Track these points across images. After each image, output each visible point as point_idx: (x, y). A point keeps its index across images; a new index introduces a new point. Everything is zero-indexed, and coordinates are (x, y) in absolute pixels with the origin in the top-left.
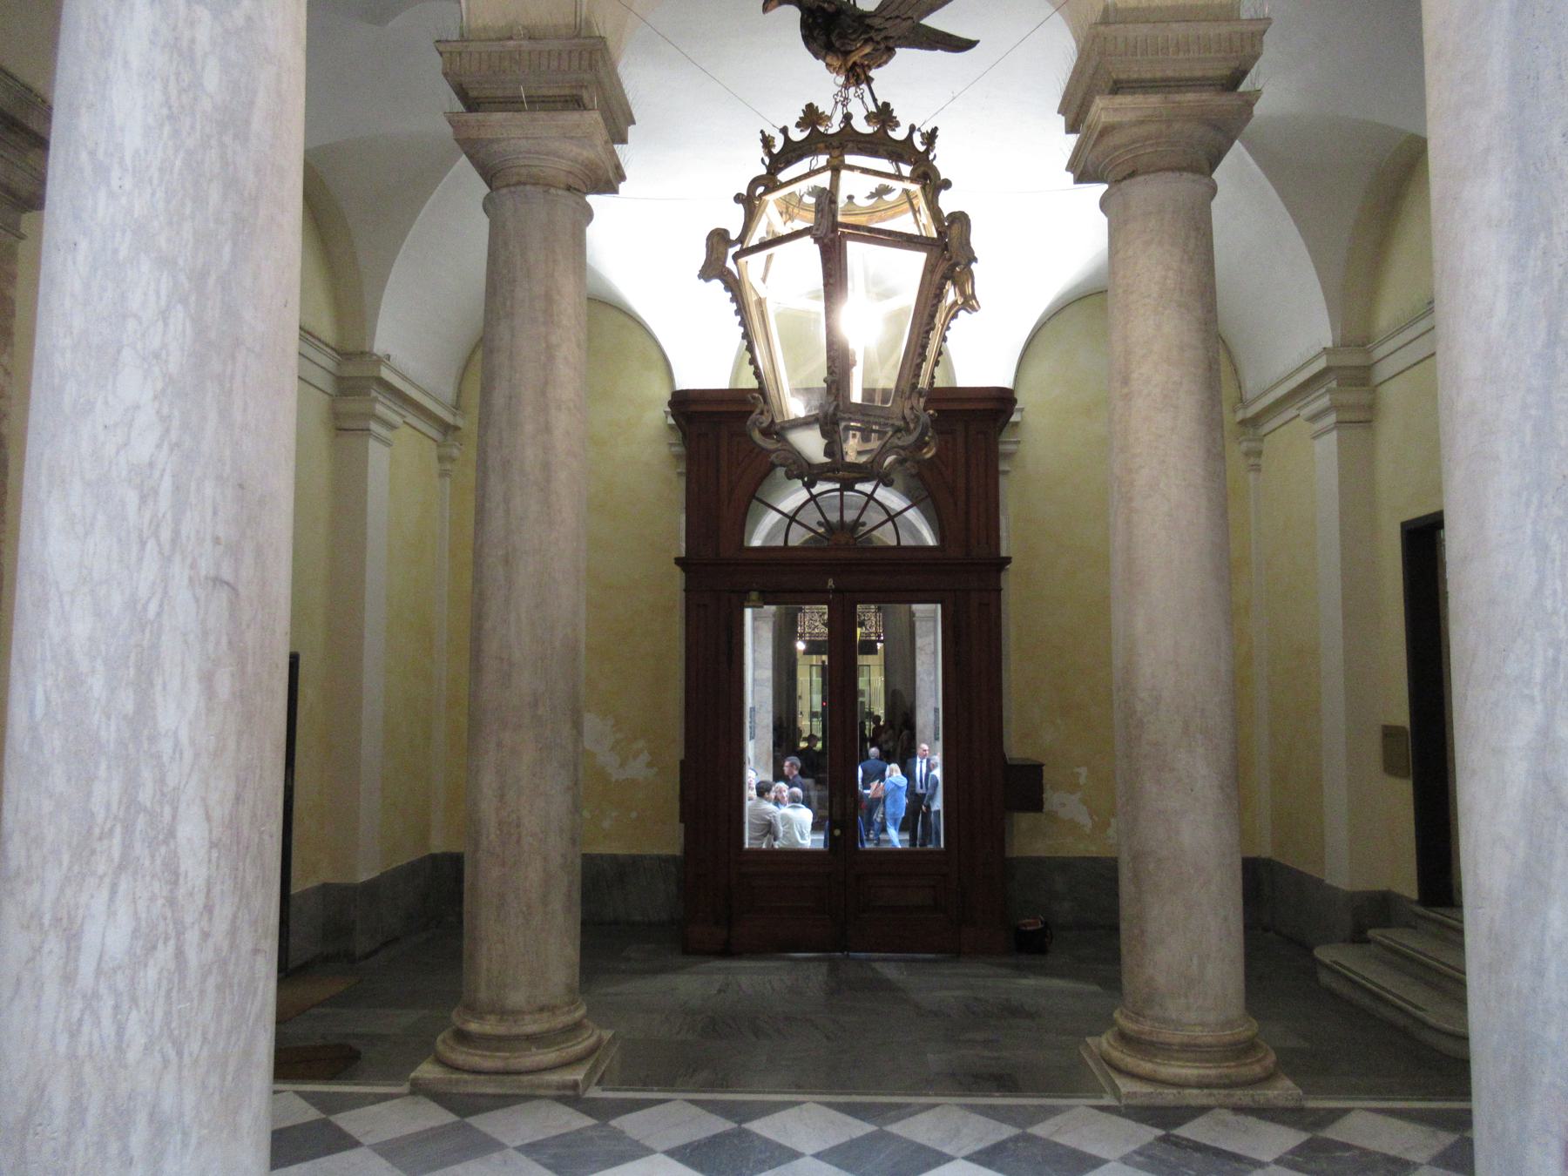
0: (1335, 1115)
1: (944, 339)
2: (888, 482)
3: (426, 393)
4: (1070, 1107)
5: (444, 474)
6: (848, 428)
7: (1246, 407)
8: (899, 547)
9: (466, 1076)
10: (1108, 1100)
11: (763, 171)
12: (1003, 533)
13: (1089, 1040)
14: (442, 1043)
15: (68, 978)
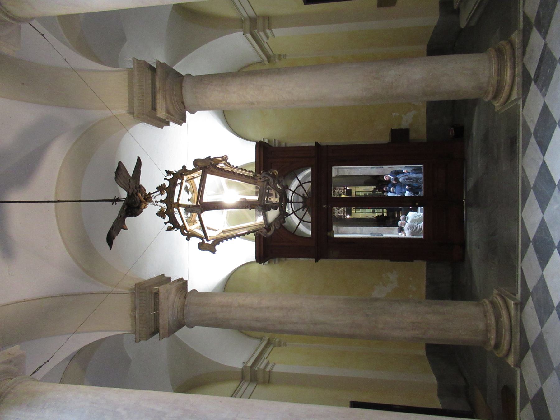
0: (526, 17)
1: (237, 167)
2: (287, 188)
3: (256, 350)
4: (523, 117)
5: (285, 345)
6: (267, 201)
7: (263, 60)
8: (312, 182)
9: (513, 345)
10: (520, 103)
11: (179, 230)
12: (307, 145)
13: (496, 110)
14: (500, 354)
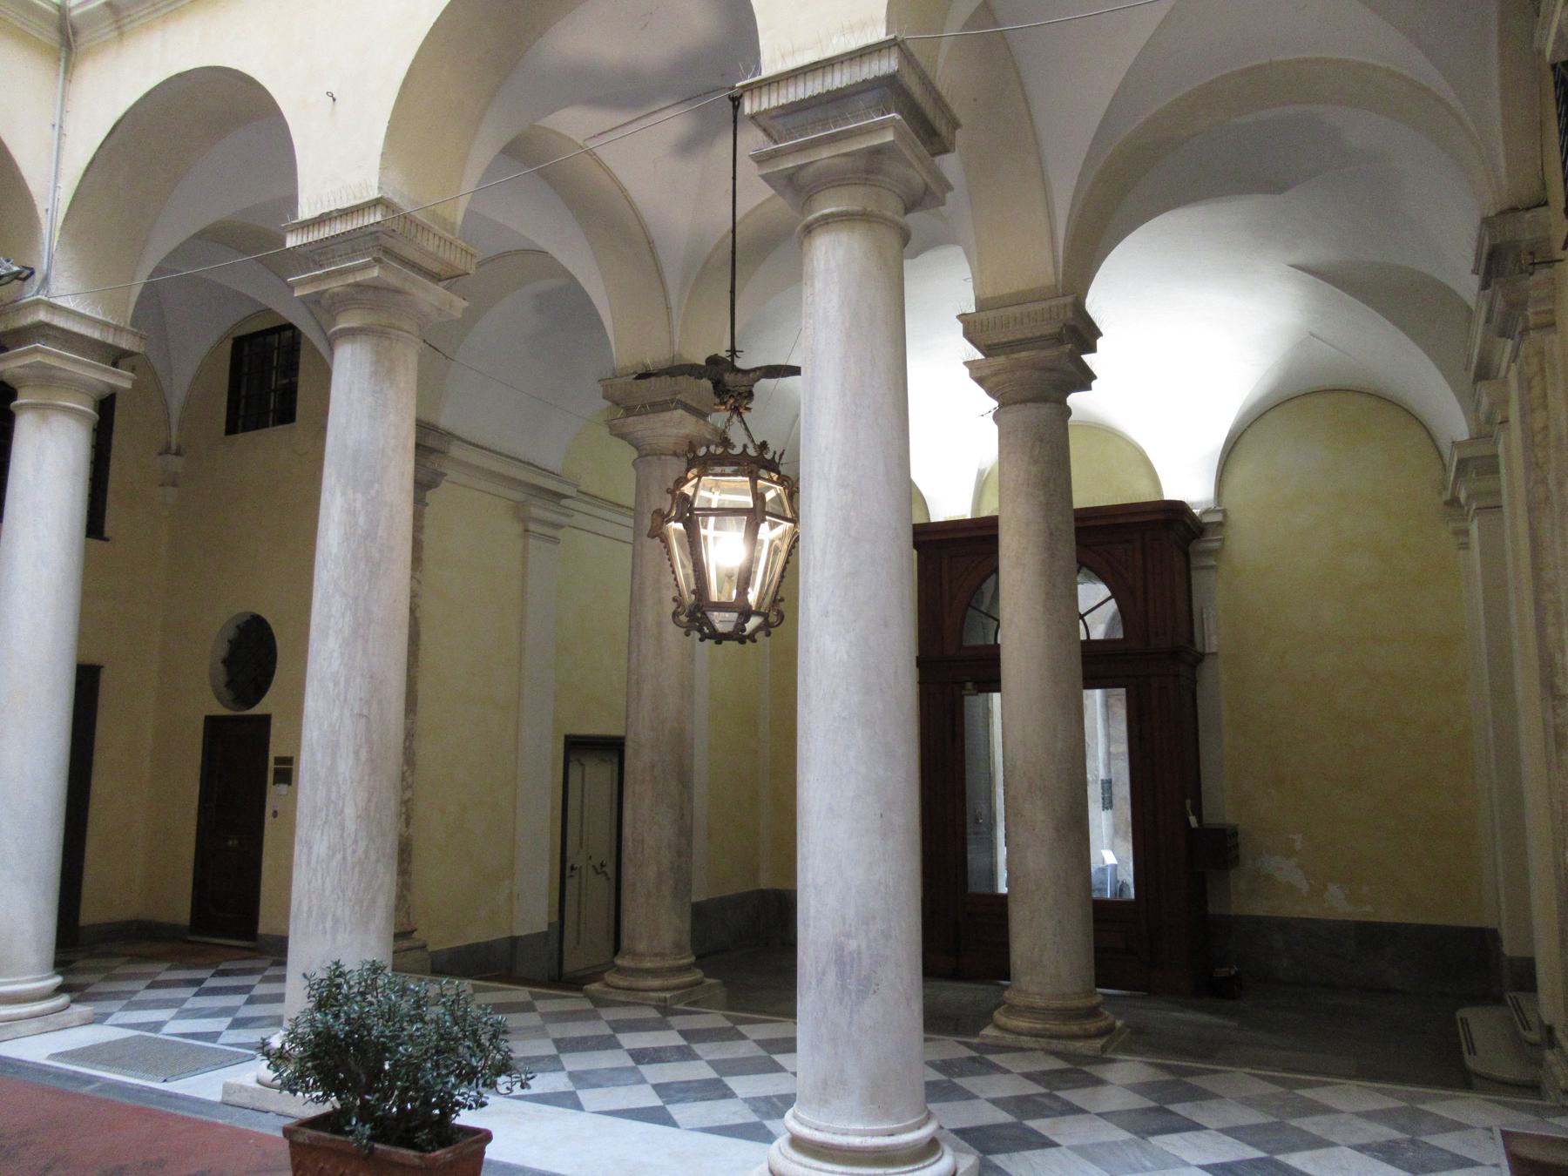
15: (309, 863)
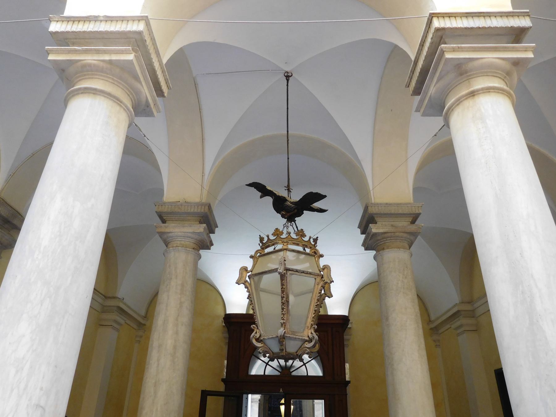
8: (307, 376)
